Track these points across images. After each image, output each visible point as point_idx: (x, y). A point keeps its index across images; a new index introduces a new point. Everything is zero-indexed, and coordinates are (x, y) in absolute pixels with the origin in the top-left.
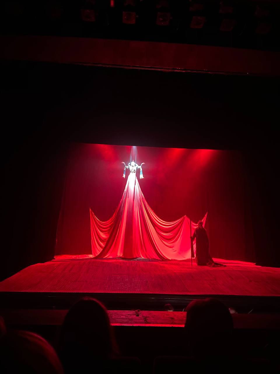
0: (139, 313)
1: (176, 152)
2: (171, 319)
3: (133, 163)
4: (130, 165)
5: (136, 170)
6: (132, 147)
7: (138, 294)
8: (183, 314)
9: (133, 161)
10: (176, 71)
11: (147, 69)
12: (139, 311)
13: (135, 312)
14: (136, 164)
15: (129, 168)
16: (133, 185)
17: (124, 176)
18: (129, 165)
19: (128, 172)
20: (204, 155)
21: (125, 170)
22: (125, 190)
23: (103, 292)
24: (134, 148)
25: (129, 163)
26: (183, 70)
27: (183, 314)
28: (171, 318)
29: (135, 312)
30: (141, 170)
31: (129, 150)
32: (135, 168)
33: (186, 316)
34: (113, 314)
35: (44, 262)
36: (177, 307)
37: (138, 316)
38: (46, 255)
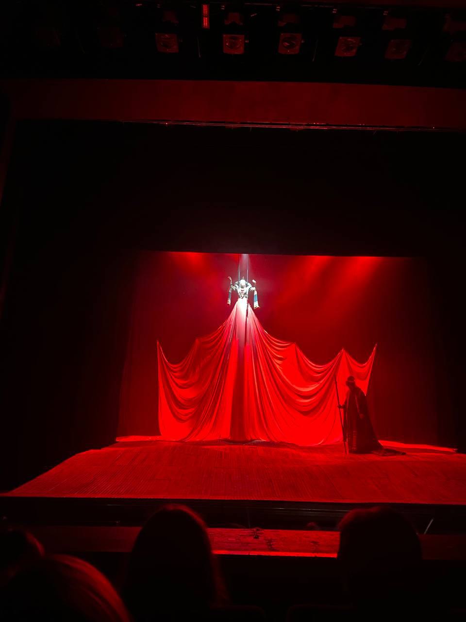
0: (259, 533)
1: (316, 262)
2: (313, 544)
3: (243, 282)
4: (238, 285)
5: (247, 293)
6: (241, 256)
7: (255, 501)
8: (333, 537)
9: (243, 278)
10: (312, 127)
11: (263, 126)
12: (258, 530)
13: (252, 531)
14: (249, 284)
15: (236, 290)
16: (243, 310)
17: (229, 302)
18: (236, 285)
19: (235, 297)
20: (361, 266)
21: (230, 291)
22: (230, 337)
23: (198, 498)
24: (245, 256)
25: (237, 283)
26: (323, 125)
27: (333, 537)
28: (313, 542)
29: (252, 531)
30: (256, 293)
31: (237, 261)
32: (246, 290)
33: (339, 539)
34: (215, 534)
35: (100, 448)
36: (326, 524)
37: (257, 537)
38: (104, 439)
